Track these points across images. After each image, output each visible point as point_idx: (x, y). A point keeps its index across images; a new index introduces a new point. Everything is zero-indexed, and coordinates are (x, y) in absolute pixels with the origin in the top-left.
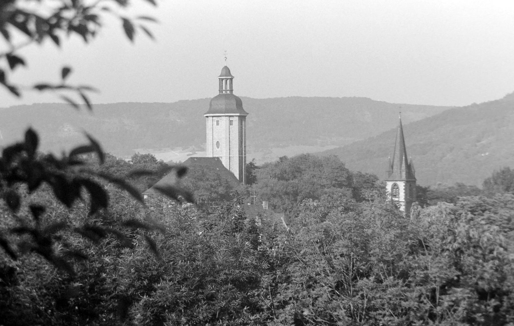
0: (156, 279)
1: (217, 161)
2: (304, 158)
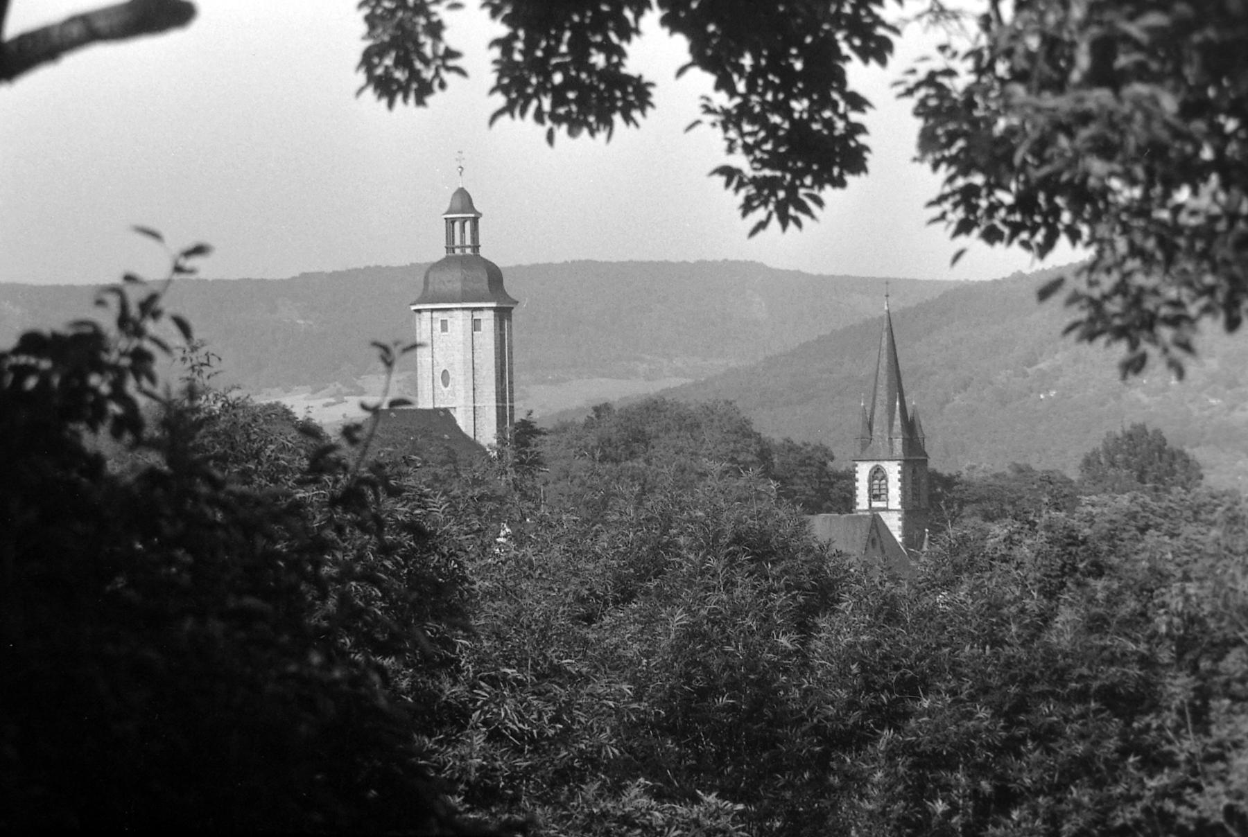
0: (912, 687)
1: (444, 417)
2: (653, 407)
